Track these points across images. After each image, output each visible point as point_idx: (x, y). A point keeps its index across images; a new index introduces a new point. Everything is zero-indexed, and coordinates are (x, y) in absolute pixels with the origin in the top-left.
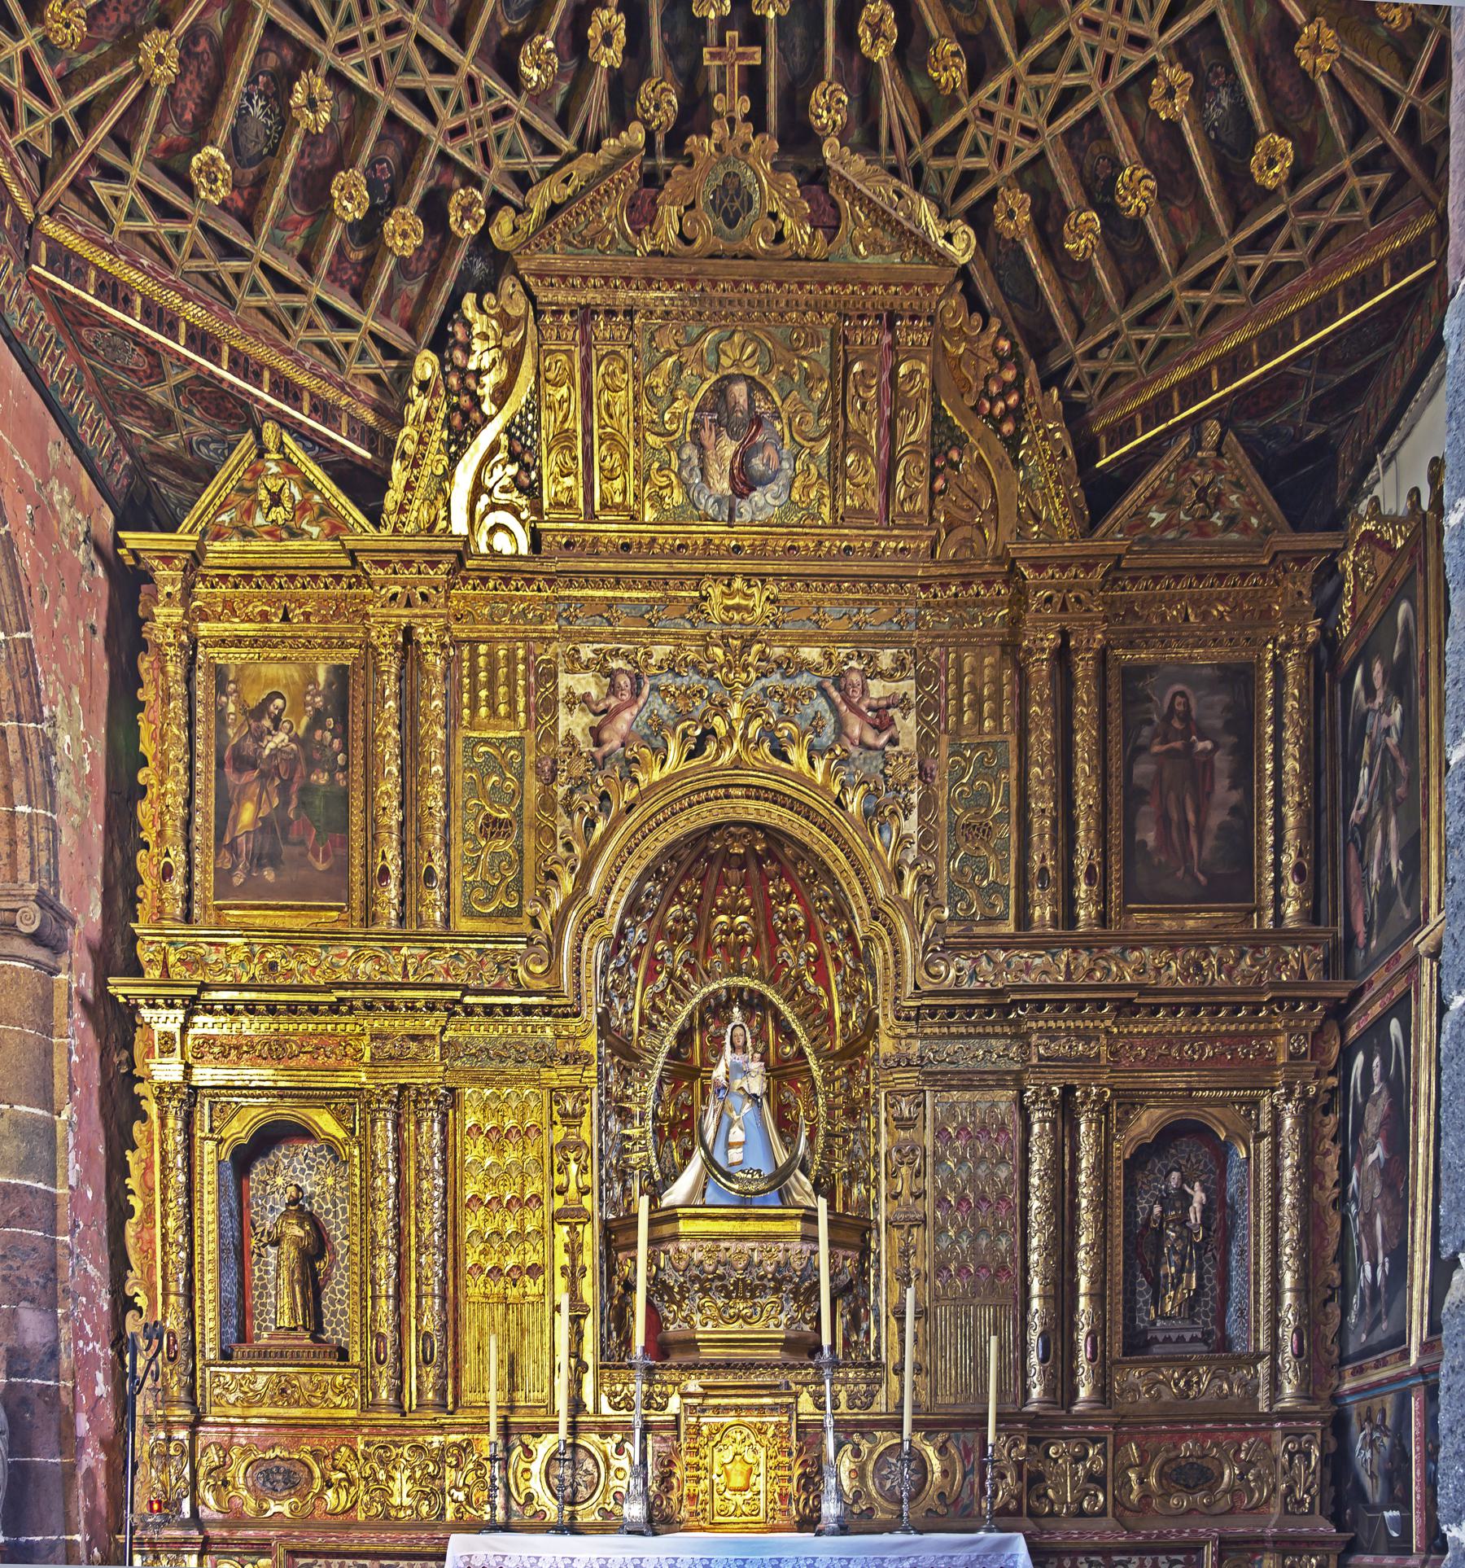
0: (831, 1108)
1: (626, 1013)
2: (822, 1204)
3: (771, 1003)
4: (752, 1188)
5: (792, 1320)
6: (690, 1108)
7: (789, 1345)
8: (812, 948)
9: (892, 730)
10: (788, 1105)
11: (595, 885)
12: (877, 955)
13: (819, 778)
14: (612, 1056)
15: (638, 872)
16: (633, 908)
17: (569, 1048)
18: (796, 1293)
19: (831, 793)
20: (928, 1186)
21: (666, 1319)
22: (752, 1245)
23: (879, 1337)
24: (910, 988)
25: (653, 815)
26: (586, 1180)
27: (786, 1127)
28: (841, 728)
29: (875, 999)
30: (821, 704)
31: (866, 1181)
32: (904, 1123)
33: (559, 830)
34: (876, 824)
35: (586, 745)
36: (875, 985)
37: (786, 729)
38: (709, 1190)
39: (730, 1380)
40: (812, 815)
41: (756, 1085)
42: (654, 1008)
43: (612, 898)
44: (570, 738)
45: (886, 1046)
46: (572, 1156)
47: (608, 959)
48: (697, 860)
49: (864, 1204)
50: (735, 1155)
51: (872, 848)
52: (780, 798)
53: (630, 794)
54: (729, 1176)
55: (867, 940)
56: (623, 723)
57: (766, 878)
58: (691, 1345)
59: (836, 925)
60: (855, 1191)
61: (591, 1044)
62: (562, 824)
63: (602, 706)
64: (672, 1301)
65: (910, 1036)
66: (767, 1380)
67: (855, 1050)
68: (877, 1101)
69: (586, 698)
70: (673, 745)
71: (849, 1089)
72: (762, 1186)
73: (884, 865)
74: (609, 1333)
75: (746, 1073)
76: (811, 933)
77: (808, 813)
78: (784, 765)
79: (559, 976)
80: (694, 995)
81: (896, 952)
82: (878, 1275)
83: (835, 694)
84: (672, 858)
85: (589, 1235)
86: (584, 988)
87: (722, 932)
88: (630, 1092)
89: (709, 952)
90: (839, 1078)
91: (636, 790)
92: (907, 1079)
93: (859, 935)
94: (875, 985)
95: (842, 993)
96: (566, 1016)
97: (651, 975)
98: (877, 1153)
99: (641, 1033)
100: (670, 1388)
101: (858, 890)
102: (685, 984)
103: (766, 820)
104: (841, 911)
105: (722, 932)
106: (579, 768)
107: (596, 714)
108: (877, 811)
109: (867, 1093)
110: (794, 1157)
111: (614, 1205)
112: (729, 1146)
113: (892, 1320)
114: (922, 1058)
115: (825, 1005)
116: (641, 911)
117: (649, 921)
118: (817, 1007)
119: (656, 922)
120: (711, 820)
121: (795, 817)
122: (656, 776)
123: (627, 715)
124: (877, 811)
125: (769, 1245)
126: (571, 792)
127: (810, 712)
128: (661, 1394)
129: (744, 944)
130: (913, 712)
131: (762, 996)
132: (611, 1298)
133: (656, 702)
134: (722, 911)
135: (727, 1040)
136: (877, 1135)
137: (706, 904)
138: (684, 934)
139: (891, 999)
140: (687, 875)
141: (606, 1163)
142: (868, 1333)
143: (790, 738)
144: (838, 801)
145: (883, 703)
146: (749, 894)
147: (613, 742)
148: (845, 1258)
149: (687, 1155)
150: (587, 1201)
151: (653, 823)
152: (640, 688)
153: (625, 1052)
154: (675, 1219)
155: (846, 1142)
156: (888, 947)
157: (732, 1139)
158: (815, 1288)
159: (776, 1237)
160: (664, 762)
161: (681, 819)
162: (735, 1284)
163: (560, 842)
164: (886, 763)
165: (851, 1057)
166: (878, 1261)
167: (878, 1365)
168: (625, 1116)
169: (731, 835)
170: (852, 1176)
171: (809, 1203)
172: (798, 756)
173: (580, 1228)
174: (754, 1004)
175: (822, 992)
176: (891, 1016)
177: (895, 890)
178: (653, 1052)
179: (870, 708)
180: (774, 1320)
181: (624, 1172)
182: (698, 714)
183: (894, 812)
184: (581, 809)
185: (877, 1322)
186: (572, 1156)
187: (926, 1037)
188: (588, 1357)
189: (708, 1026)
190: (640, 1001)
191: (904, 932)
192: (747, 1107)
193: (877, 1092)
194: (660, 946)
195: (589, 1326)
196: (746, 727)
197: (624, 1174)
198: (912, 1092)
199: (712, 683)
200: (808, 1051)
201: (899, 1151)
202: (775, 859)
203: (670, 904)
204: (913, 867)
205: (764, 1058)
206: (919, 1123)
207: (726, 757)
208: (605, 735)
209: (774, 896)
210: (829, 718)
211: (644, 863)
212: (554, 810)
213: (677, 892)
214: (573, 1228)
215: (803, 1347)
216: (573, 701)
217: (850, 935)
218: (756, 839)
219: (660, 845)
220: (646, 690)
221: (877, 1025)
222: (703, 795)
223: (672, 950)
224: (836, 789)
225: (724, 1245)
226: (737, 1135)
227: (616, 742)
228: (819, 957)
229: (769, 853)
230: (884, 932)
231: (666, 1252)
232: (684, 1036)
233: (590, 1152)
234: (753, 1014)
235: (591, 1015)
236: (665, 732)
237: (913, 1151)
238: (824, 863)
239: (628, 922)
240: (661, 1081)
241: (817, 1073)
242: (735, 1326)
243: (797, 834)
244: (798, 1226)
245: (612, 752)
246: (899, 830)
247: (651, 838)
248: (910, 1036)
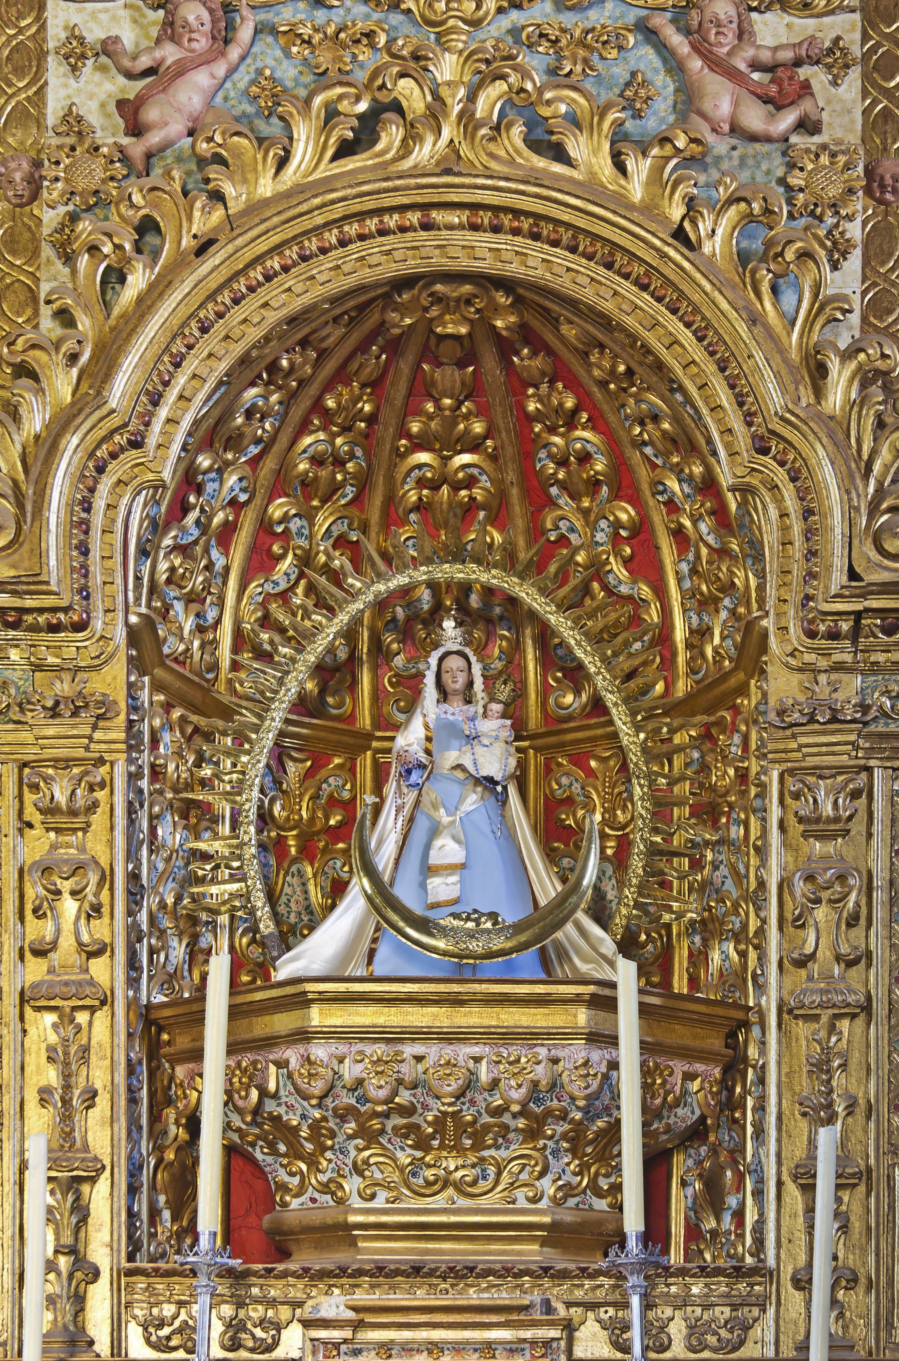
0: (661, 807)
1: (200, 629)
2: (626, 975)
3: (532, 615)
4: (475, 946)
5: (568, 1190)
6: (349, 806)
7: (556, 1235)
8: (625, 513)
9: (806, 106)
10: (569, 801)
11: (121, 388)
12: (767, 521)
13: (636, 191)
14: (168, 707)
15: (223, 367)
16: (215, 434)
17: (64, 687)
18: (575, 1141)
19: (664, 220)
20: (877, 941)
21: (283, 1188)
22: (476, 1050)
23: (761, 1222)
24: (838, 579)
25: (258, 260)
26: (100, 929)
27: (558, 837)
28: (688, 101)
29: (761, 601)
30: (646, 58)
31: (739, 936)
32: (817, 827)
33: (45, 288)
34: (766, 279)
35: (108, 132)
36: (761, 575)
37: (560, 103)
38: (384, 951)
39: (421, 1297)
40: (620, 259)
41: (494, 761)
42: (266, 621)
43: (163, 412)
44: (73, 122)
45: (782, 685)
46: (66, 886)
47: (157, 527)
48: (363, 347)
49: (736, 978)
50: (442, 888)
51: (754, 319)
52: (546, 229)
53: (204, 220)
54: (424, 925)
55: (744, 491)
56: (192, 93)
57: (518, 384)
58: (341, 1233)
59: (678, 471)
60: (716, 957)
61: (113, 680)
62: (52, 277)
63: (145, 62)
64: (296, 1153)
65: (839, 667)
66: (503, 1297)
67: (716, 700)
68: (763, 788)
69: (108, 48)
70: (304, 134)
71: (704, 768)
72: (498, 943)
73: (782, 351)
74: (154, 1214)
75: (472, 739)
76: (623, 484)
77: (611, 257)
78: (558, 168)
79: (40, 555)
80: (354, 595)
81: (808, 513)
82: (760, 1107)
83: (677, 40)
84: (304, 343)
85: (106, 1032)
86: (97, 576)
87: (421, 483)
88: (207, 772)
89: (392, 516)
90: (680, 749)
91: (218, 214)
92: (836, 747)
93: (725, 479)
94: (761, 575)
95: (688, 595)
96: (54, 628)
97: (260, 561)
98: (762, 885)
99: (235, 666)
100: (285, 1312)
101: (724, 398)
102: (336, 578)
103: (515, 269)
104: (686, 443)
105: (421, 483)
106: (93, 174)
107: (130, 76)
108: (772, 252)
109: (743, 776)
110: (572, 889)
111: (171, 979)
112: (428, 870)
113: (792, 1190)
114: (865, 708)
115: (653, 615)
116: (234, 442)
117: (255, 462)
118: (636, 620)
119: (269, 464)
120: (390, 270)
121: (578, 263)
122: (266, 187)
123: (202, 78)
124: (772, 252)
125: (514, 1051)
126: (73, 218)
127: (621, 73)
128: (262, 1323)
129: (472, 506)
130: (855, 73)
131: (513, 601)
132: (159, 1149)
133: (269, 55)
134: (419, 445)
135: (430, 679)
136: (762, 851)
137: (386, 430)
138: (335, 488)
139: (794, 596)
140: (341, 376)
141: (150, 902)
142: (739, 1215)
143: (574, 121)
144: (679, 234)
145: (787, 55)
146: (482, 412)
147: (168, 119)
148: (689, 1077)
149: (338, 889)
150: (99, 968)
151: (257, 274)
152: (231, 27)
153: (202, 705)
154: (302, 1001)
155: (697, 864)
156: (791, 503)
157: (434, 859)
158: (613, 1133)
159: (531, 1036)
160: (282, 163)
161: (322, 267)
162: (439, 1123)
163: (46, 312)
164: (791, 166)
165: (710, 710)
166: (762, 1081)
167: (771, 1275)
168: (195, 815)
169: (438, 299)
170: (708, 928)
171: (605, 973)
172: (589, 153)
173: (82, 1018)
174: (491, 615)
175: (645, 591)
176: (795, 631)
177: (807, 396)
178: (262, 704)
179: (755, 66)
180: (528, 1189)
181: (193, 920)
182: (361, 76)
183: (805, 255)
184: (93, 249)
185: (759, 1193)
186: (66, 886)
187: (875, 668)
188: (101, 1249)
189: (389, 656)
190: (236, 606)
191: (828, 476)
192: (472, 800)
193: (764, 771)
194: (278, 508)
195: (101, 1199)
196: (472, 98)
197: (193, 924)
198: (841, 769)
199: (396, 19)
200: (610, 699)
201: (810, 878)
202: (538, 346)
203: (303, 428)
204: (847, 355)
205: (513, 711)
206: (858, 827)
207: (425, 152)
208: (151, 114)
209: (538, 417)
210: (664, 85)
211: (238, 349)
212: (36, 253)
213: (318, 406)
214: (67, 1018)
215: (585, 1238)
216: (77, 53)
217: (708, 486)
218: (497, 309)
219: (273, 317)
220: (245, 33)
221: (763, 647)
222: (372, 224)
223: (309, 516)
224: (677, 212)
225: (409, 1050)
226: (446, 850)
227: (177, 127)
228: (641, 531)
229: (526, 335)
230: (781, 476)
231: (281, 1064)
232: (334, 674)
233: (106, 878)
234: (490, 635)
235: (112, 628)
236: (287, 108)
237: (841, 878)
238: (647, 350)
239: (204, 461)
240: (280, 754)
241: (631, 739)
242: (439, 1201)
243: (588, 294)
244: (582, 1017)
245: (163, 148)
246: (817, 287)
247: (252, 303)
248: (839, 667)
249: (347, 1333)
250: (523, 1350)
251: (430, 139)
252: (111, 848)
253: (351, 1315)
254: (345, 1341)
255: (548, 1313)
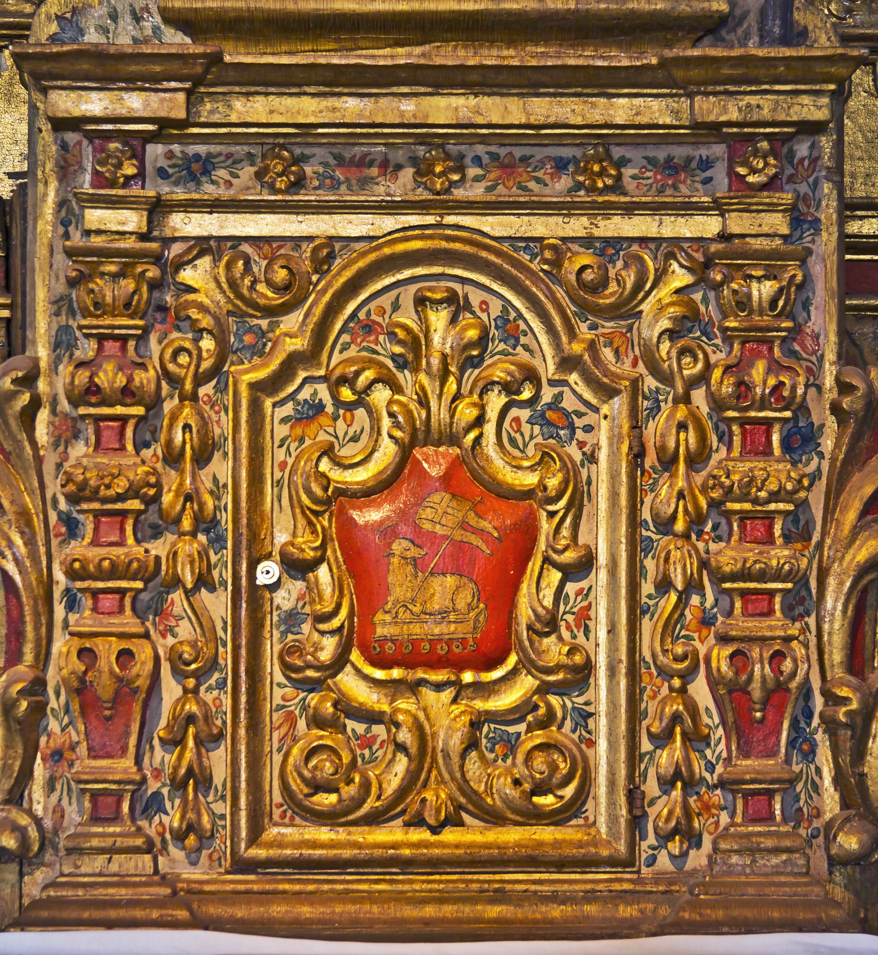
249: (170, 103)
250: (706, 164)
251: (161, 733)
252: (109, 613)
253: (176, 40)
254: (165, 128)
255: (786, 41)
